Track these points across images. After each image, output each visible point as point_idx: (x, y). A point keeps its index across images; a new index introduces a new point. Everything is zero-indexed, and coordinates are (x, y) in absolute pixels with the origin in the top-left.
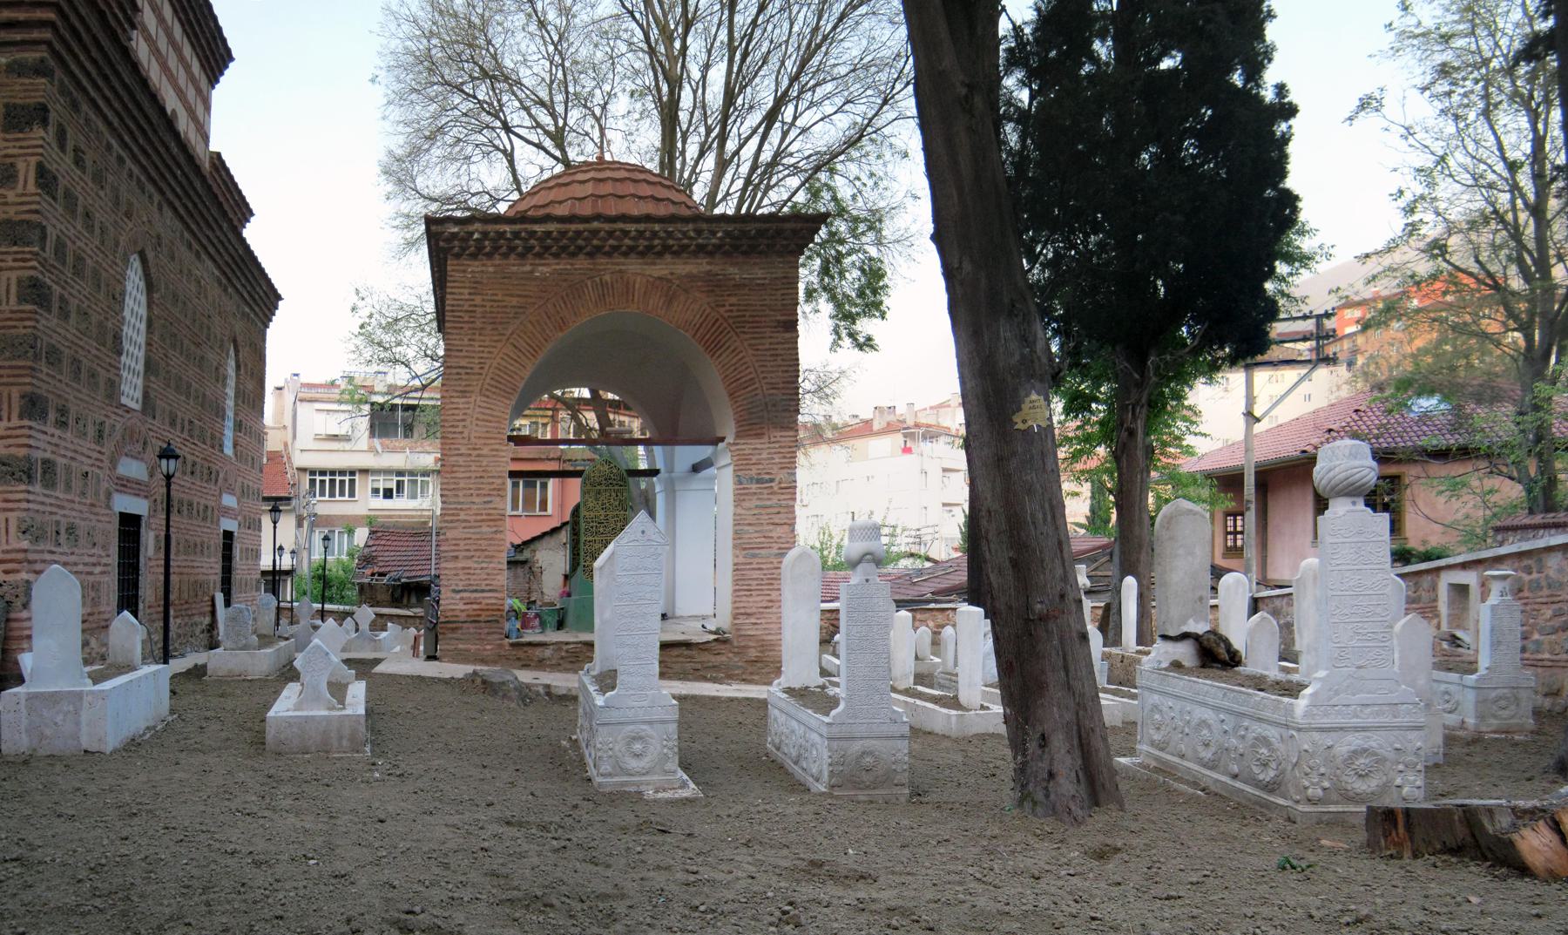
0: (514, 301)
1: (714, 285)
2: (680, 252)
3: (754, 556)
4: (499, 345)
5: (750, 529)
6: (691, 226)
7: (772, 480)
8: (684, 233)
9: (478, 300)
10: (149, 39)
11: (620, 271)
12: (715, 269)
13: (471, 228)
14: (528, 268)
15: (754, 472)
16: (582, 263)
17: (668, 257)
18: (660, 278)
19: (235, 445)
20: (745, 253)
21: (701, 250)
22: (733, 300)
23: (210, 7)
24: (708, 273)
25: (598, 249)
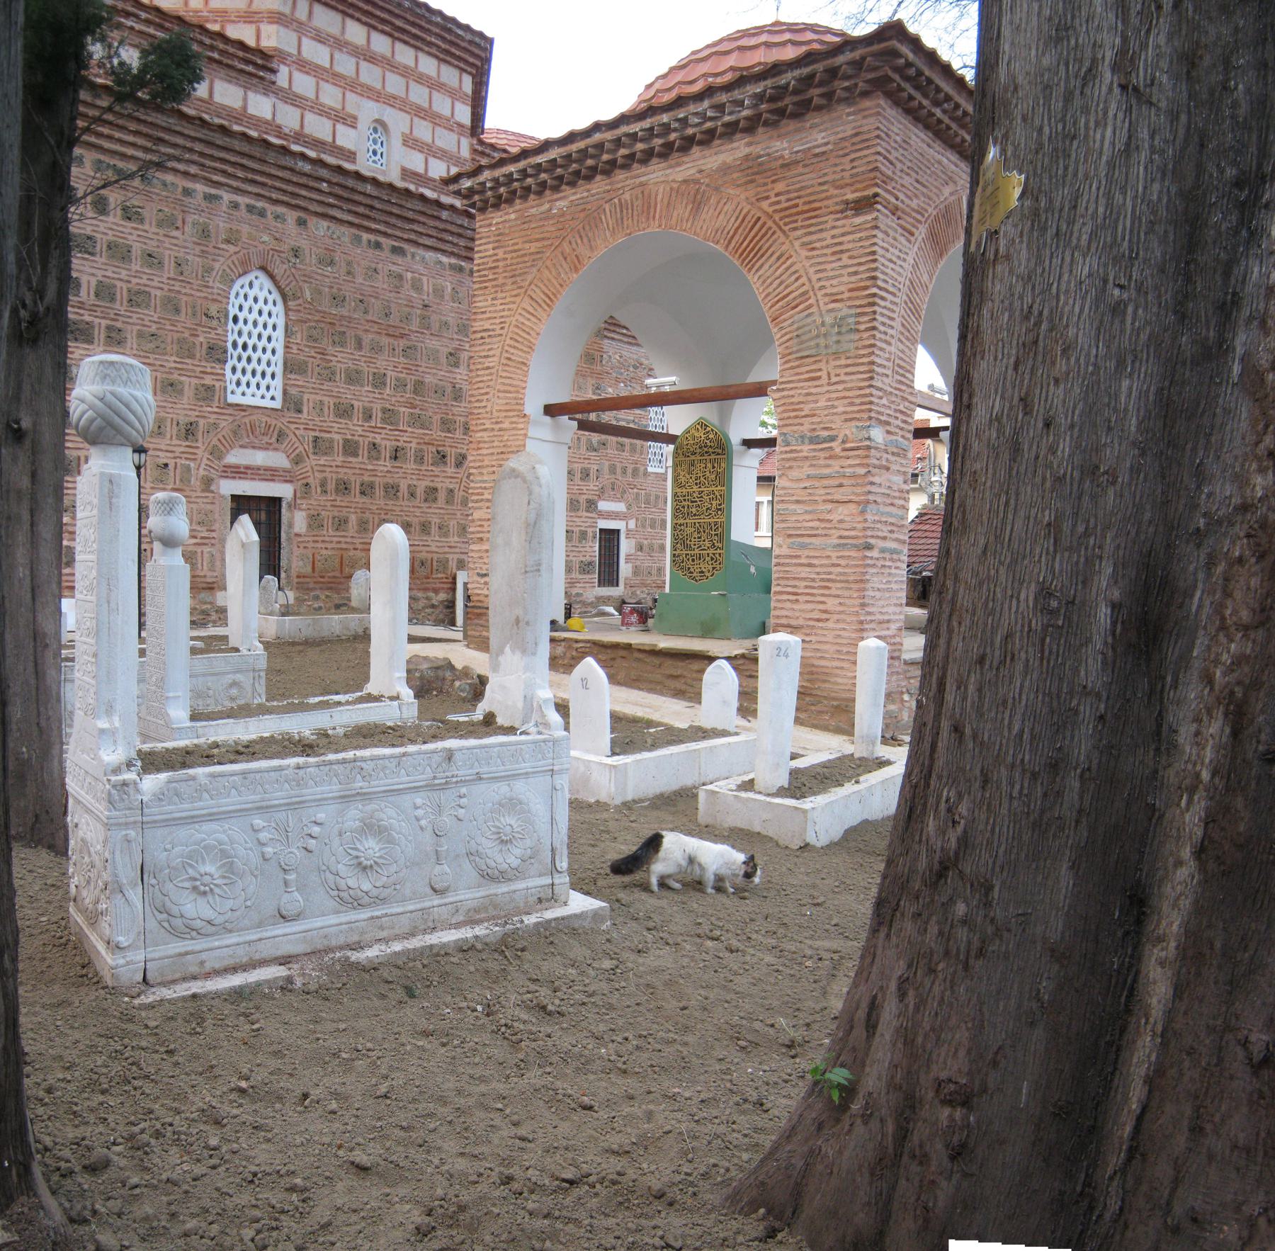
0: (534, 247)
1: (754, 171)
2: (708, 138)
3: (803, 546)
4: (518, 300)
5: (799, 508)
6: (706, 103)
7: (832, 439)
8: (703, 116)
9: (500, 252)
10: (304, 66)
11: (642, 185)
12: (757, 150)
13: (481, 178)
14: (547, 206)
15: (807, 427)
16: (599, 185)
17: (696, 151)
18: (685, 181)
19: (1012, 44)
20: (796, 116)
21: (732, 130)
22: (780, 187)
23: (426, 7)
24: (747, 157)
25: (613, 164)
